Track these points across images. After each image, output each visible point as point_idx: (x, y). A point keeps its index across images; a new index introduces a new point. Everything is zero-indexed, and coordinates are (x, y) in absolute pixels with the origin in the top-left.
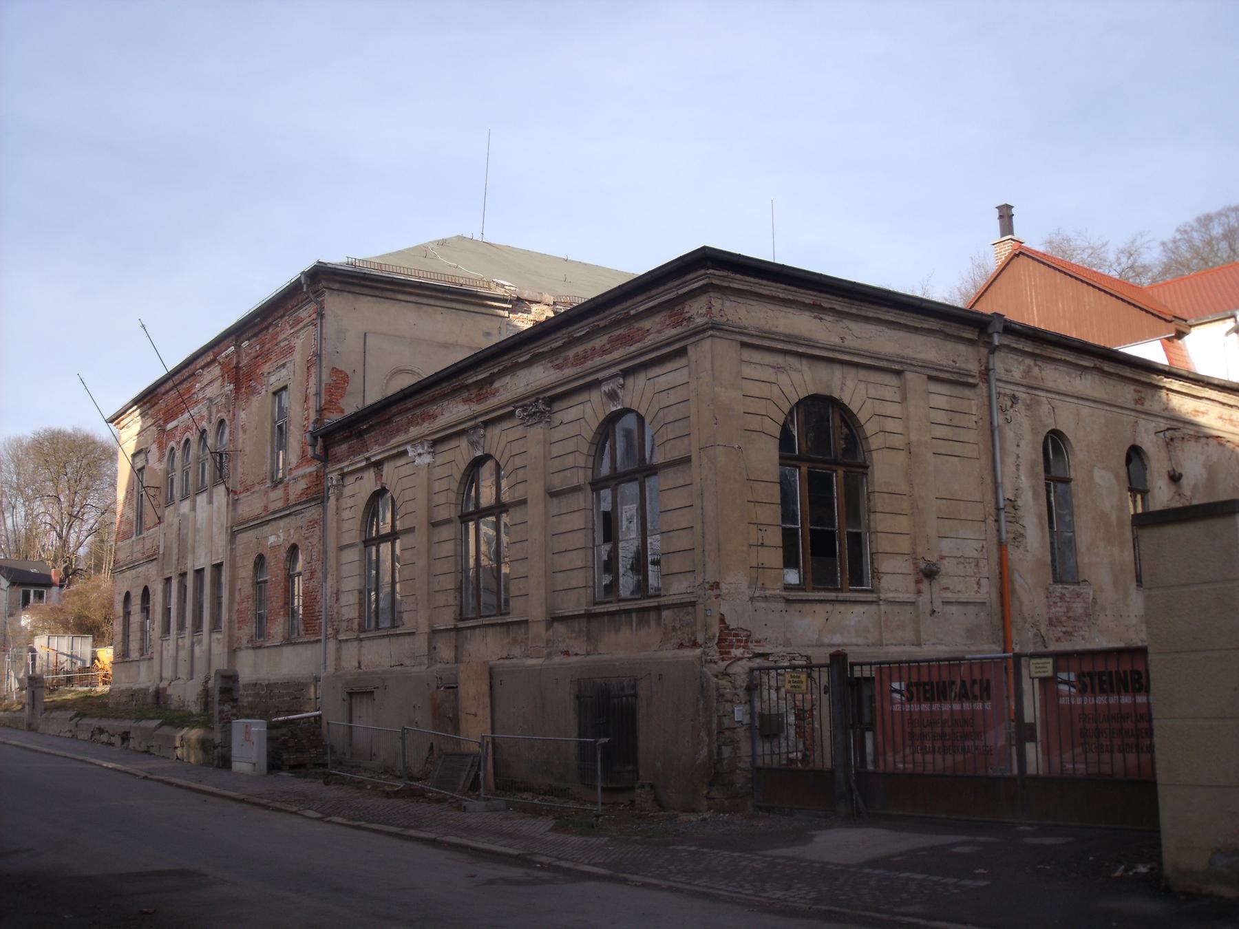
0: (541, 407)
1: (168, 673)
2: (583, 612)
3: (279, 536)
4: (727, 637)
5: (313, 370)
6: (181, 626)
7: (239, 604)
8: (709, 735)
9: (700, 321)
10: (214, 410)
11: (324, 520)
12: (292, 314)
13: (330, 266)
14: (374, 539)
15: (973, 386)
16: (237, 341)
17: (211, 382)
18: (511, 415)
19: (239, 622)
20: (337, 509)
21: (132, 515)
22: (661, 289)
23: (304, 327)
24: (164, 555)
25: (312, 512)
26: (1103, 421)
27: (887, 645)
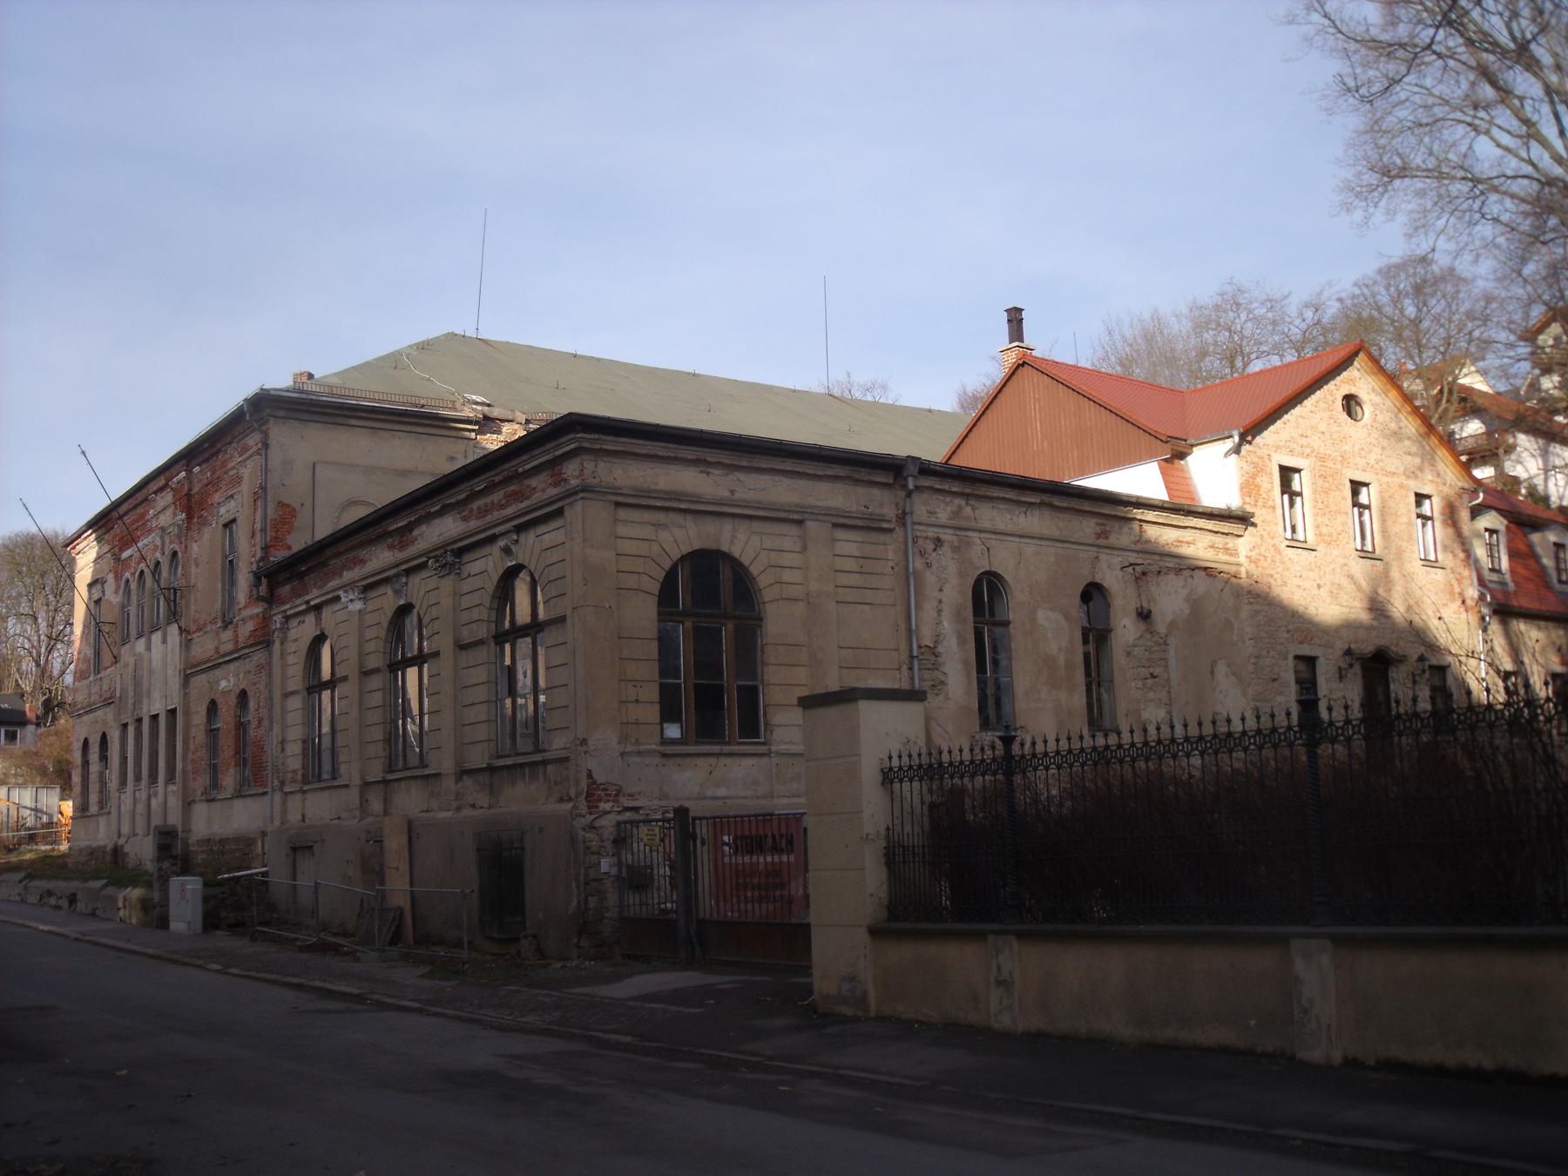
0: (450, 559)
1: (126, 829)
2: (485, 766)
3: (229, 681)
4: (594, 793)
5: (259, 503)
6: (138, 778)
7: (193, 754)
8: (578, 886)
9: (574, 482)
10: (167, 541)
11: (270, 664)
12: (239, 442)
13: (273, 393)
14: (507, 633)
15: (890, 530)
16: (187, 466)
17: (164, 509)
18: (423, 566)
20: (282, 654)
21: (90, 652)
22: (541, 450)
23: (251, 456)
25: (259, 657)
26: (1052, 559)
27: (778, 797)
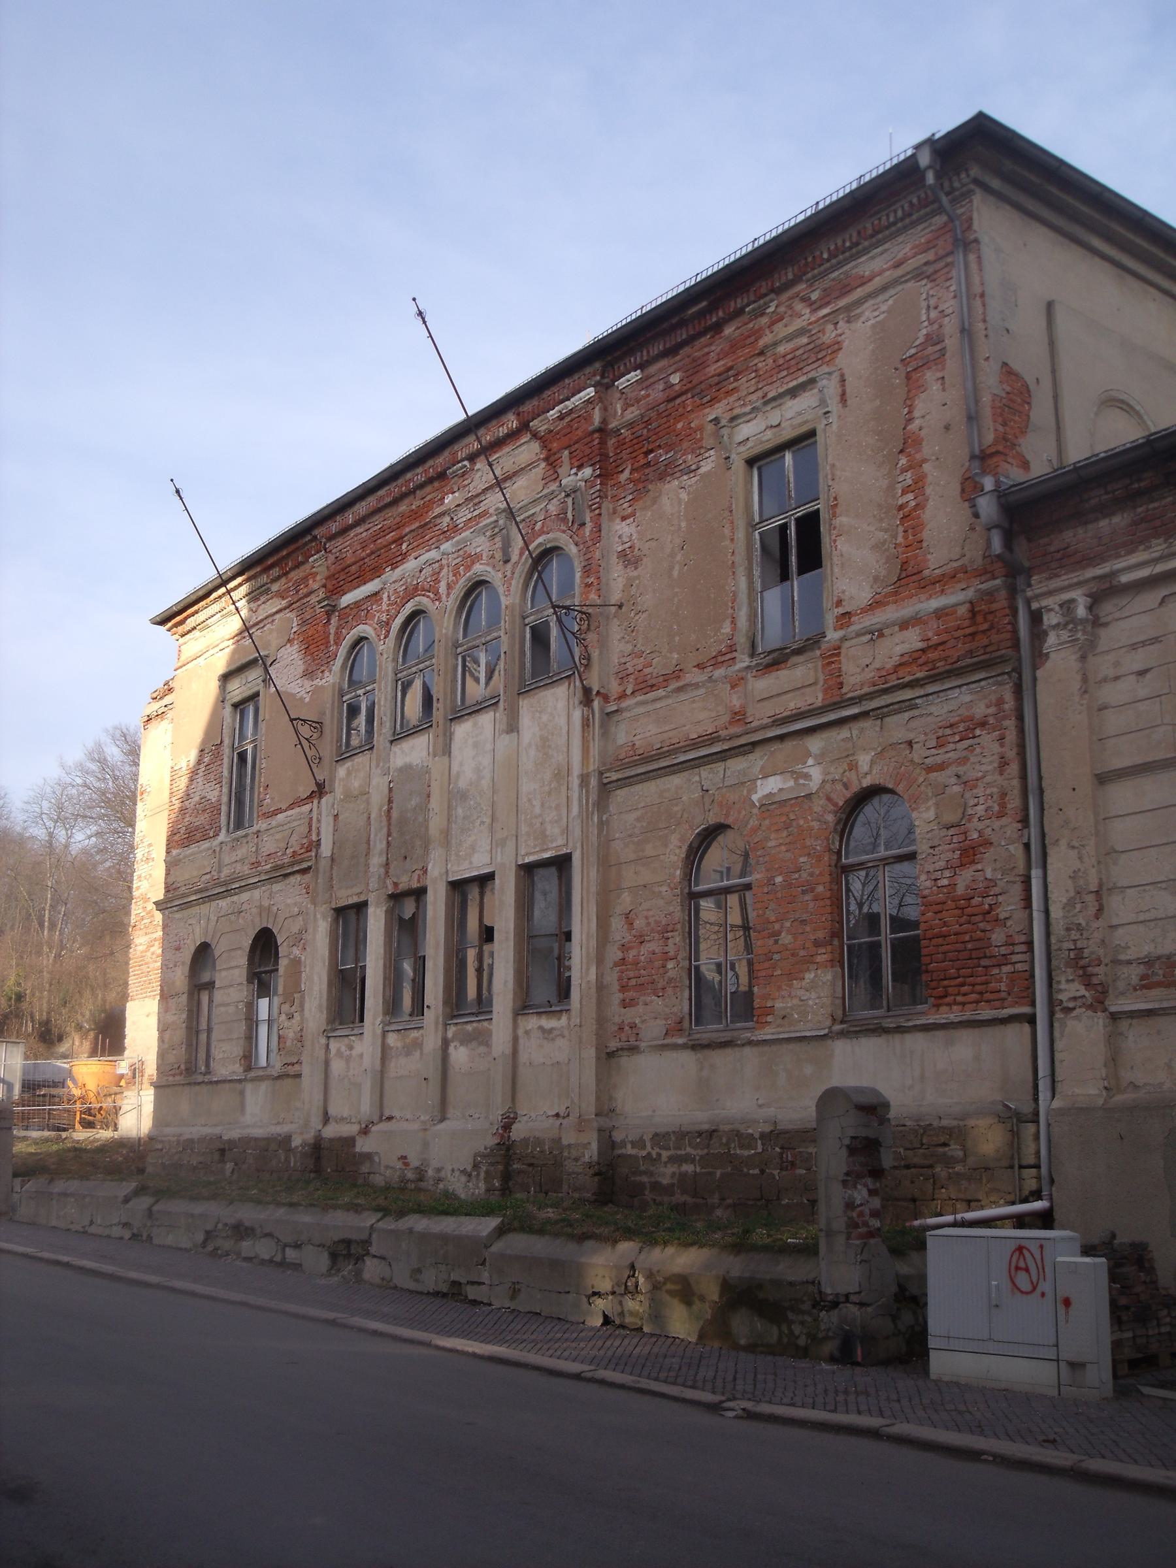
19: (623, 988)
24: (333, 860)
